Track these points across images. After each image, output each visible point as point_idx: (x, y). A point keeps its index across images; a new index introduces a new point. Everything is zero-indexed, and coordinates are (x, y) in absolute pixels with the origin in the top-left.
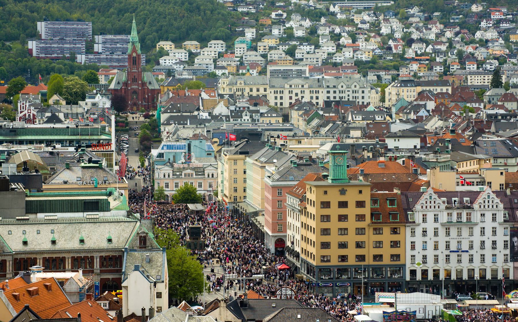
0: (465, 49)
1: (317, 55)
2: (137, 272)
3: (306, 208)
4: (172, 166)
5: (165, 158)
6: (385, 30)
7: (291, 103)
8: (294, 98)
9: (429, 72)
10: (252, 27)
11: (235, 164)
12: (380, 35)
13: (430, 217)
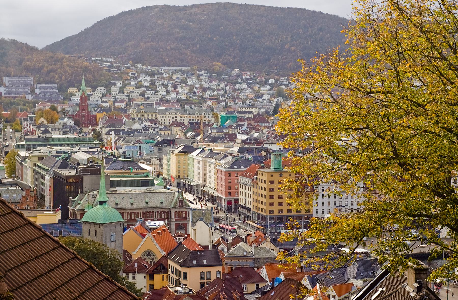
2: (202, 222)
3: (258, 184)
6: (190, 83)
7: (170, 123)
8: (171, 120)
9: (218, 106)
10: (120, 80)
11: (179, 158)
12: (188, 85)
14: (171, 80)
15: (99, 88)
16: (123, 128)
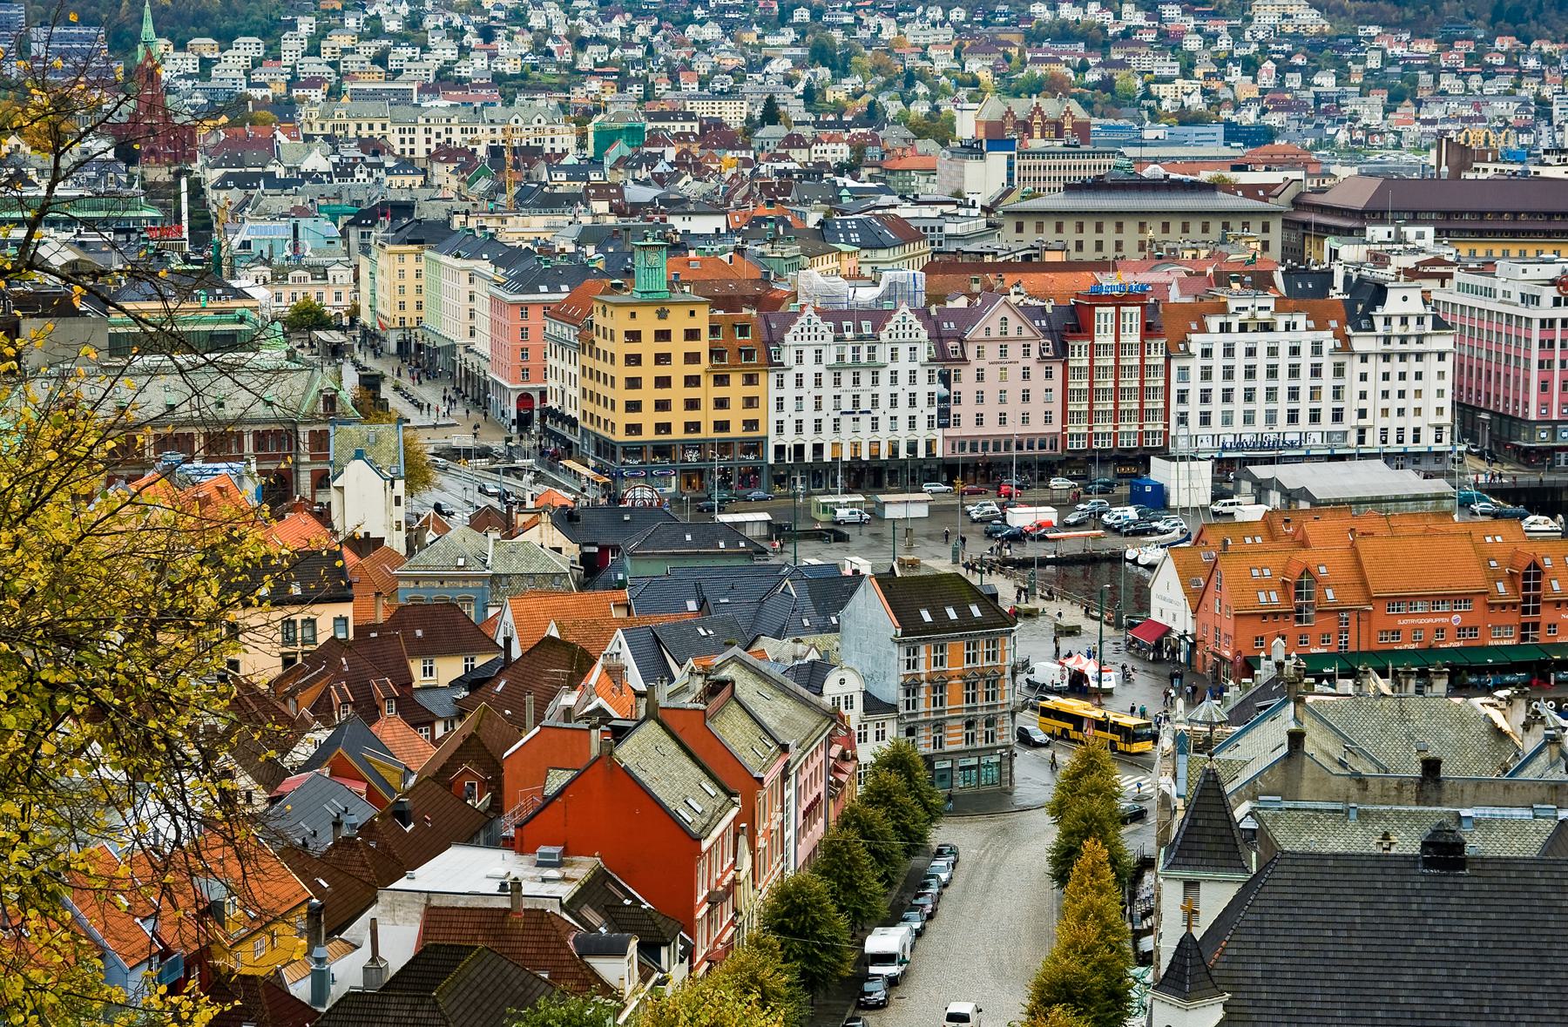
0: (673, 54)
1: (428, 65)
2: (360, 462)
4: (268, 263)
5: (255, 249)
6: (537, 21)
7: (428, 151)
8: (434, 141)
12: (530, 30)
13: (809, 355)
14: (476, 14)
15: (241, 40)
16: (270, 168)
